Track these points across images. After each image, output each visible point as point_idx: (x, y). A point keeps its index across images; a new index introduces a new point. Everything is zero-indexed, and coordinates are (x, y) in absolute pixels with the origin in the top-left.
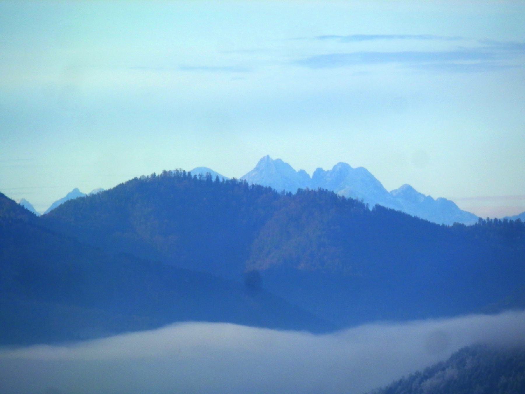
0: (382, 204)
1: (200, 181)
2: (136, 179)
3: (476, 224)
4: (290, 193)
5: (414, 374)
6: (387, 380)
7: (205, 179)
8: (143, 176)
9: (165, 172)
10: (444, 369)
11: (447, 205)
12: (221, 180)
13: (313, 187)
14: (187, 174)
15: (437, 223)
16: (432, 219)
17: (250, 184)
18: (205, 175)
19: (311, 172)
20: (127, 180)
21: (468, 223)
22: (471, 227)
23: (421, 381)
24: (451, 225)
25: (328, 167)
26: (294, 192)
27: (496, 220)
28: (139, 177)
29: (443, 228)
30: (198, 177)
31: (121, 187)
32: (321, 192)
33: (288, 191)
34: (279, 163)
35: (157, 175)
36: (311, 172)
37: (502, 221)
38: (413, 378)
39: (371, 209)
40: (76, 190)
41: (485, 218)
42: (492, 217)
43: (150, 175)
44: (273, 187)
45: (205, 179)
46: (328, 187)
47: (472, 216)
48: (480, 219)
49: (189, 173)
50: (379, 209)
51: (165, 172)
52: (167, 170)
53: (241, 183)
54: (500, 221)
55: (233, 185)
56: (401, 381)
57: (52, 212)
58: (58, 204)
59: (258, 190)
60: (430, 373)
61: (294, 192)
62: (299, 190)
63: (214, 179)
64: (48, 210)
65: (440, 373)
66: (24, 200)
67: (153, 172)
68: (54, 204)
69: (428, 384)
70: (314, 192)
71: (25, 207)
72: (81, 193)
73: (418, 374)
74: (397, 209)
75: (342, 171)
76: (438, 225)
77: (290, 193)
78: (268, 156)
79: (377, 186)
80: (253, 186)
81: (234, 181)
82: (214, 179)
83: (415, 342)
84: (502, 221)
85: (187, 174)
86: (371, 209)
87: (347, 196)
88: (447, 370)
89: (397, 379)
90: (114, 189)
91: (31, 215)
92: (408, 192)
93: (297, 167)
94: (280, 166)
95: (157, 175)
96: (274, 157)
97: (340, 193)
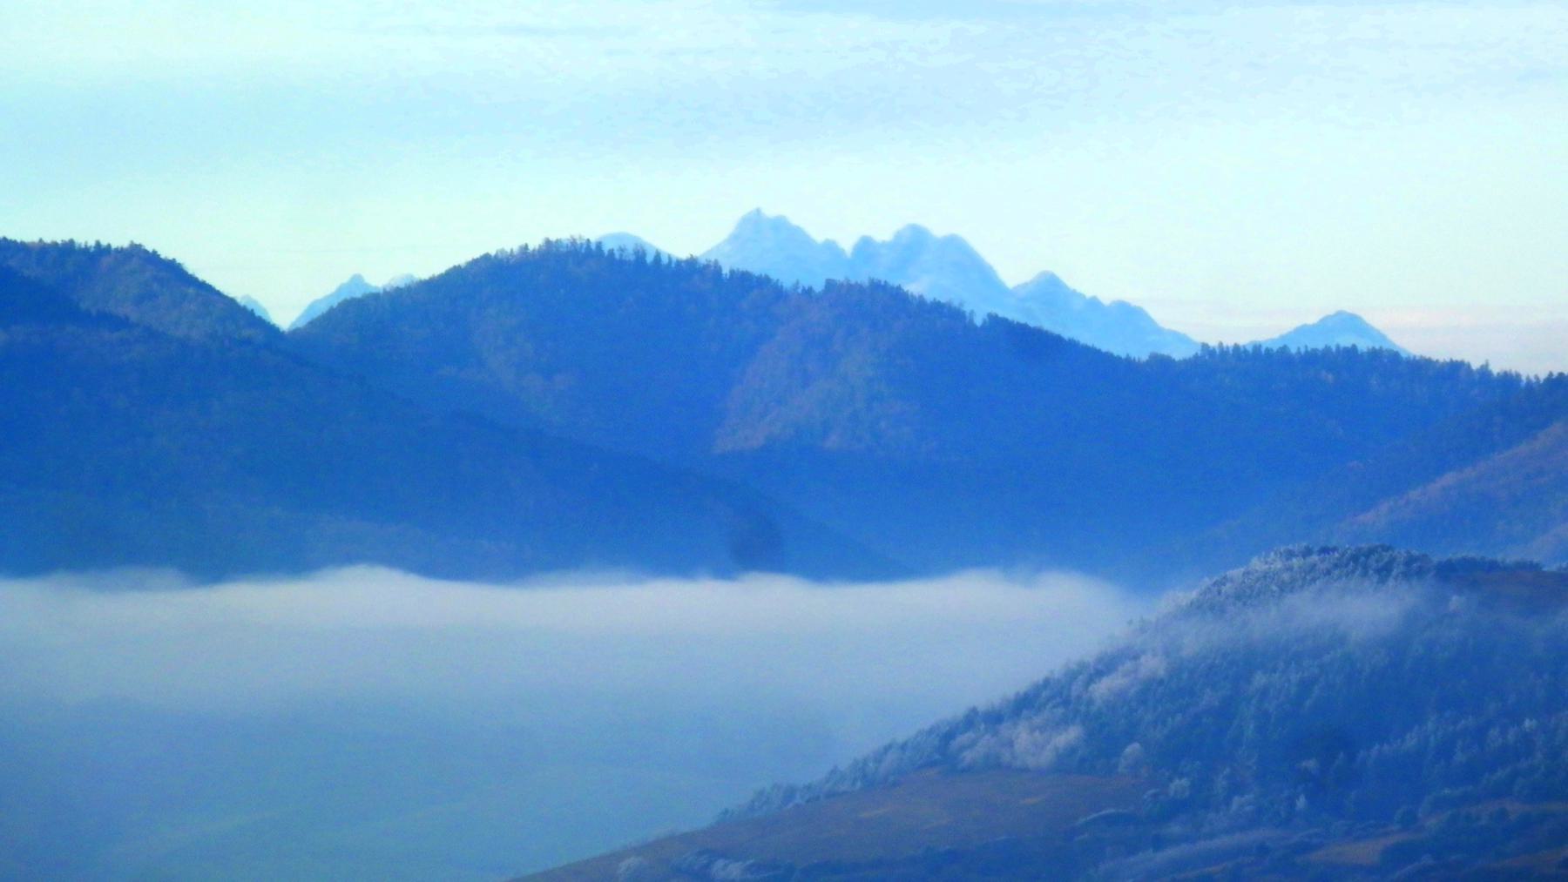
0: (1001, 313)
1: (622, 263)
2: (486, 257)
3: (1196, 356)
4: (810, 289)
5: (1074, 667)
6: (696, 805)
7: (632, 258)
8: (502, 251)
9: (548, 242)
10: (1136, 657)
11: (1128, 314)
12: (665, 261)
13: (862, 277)
14: (593, 247)
15: (1116, 353)
16: (1105, 345)
17: (726, 271)
18: (630, 249)
19: (847, 244)
20: (469, 258)
21: (1179, 354)
22: (1186, 362)
23: (1090, 680)
24: (1144, 357)
25: (883, 233)
26: (819, 287)
27: (1236, 347)
28: (493, 253)
29: (1129, 365)
30: (617, 256)
31: (456, 272)
32: (877, 286)
33: (806, 282)
34: (780, 224)
35: (531, 248)
36: (847, 244)
37: (1250, 349)
38: (1071, 676)
39: (978, 321)
40: (357, 280)
41: (1213, 343)
42: (1229, 342)
43: (516, 249)
44: (774, 276)
45: (632, 258)
46: (881, 273)
47: (1182, 339)
48: (1205, 346)
49: (599, 245)
50: (994, 320)
51: (548, 242)
52: (553, 238)
53: (707, 266)
54: (1246, 351)
55: (690, 269)
56: (1047, 682)
57: (312, 323)
58: (323, 309)
59: (743, 280)
60: (1105, 666)
61: (819, 287)
62: (830, 284)
63: (649, 259)
64: (299, 319)
65: (1129, 665)
66: (247, 297)
67: (522, 242)
68: (312, 306)
69: (1102, 689)
70: (859, 288)
71: (258, 313)
72: (367, 285)
73: (1083, 666)
74: (1032, 324)
75: (914, 242)
76: (1119, 358)
77: (810, 289)
78: (758, 211)
79: (982, 273)
80: (732, 272)
81: (692, 262)
82: (649, 259)
83: (974, 635)
84: (1250, 349)
85: (593, 247)
86: (978, 321)
87: (929, 298)
88: (1143, 659)
89: (1039, 676)
90: (441, 277)
91: (271, 330)
92: (1050, 288)
93: (818, 235)
94: (960, 257)
95: (531, 248)
96: (770, 212)
97: (914, 288)
